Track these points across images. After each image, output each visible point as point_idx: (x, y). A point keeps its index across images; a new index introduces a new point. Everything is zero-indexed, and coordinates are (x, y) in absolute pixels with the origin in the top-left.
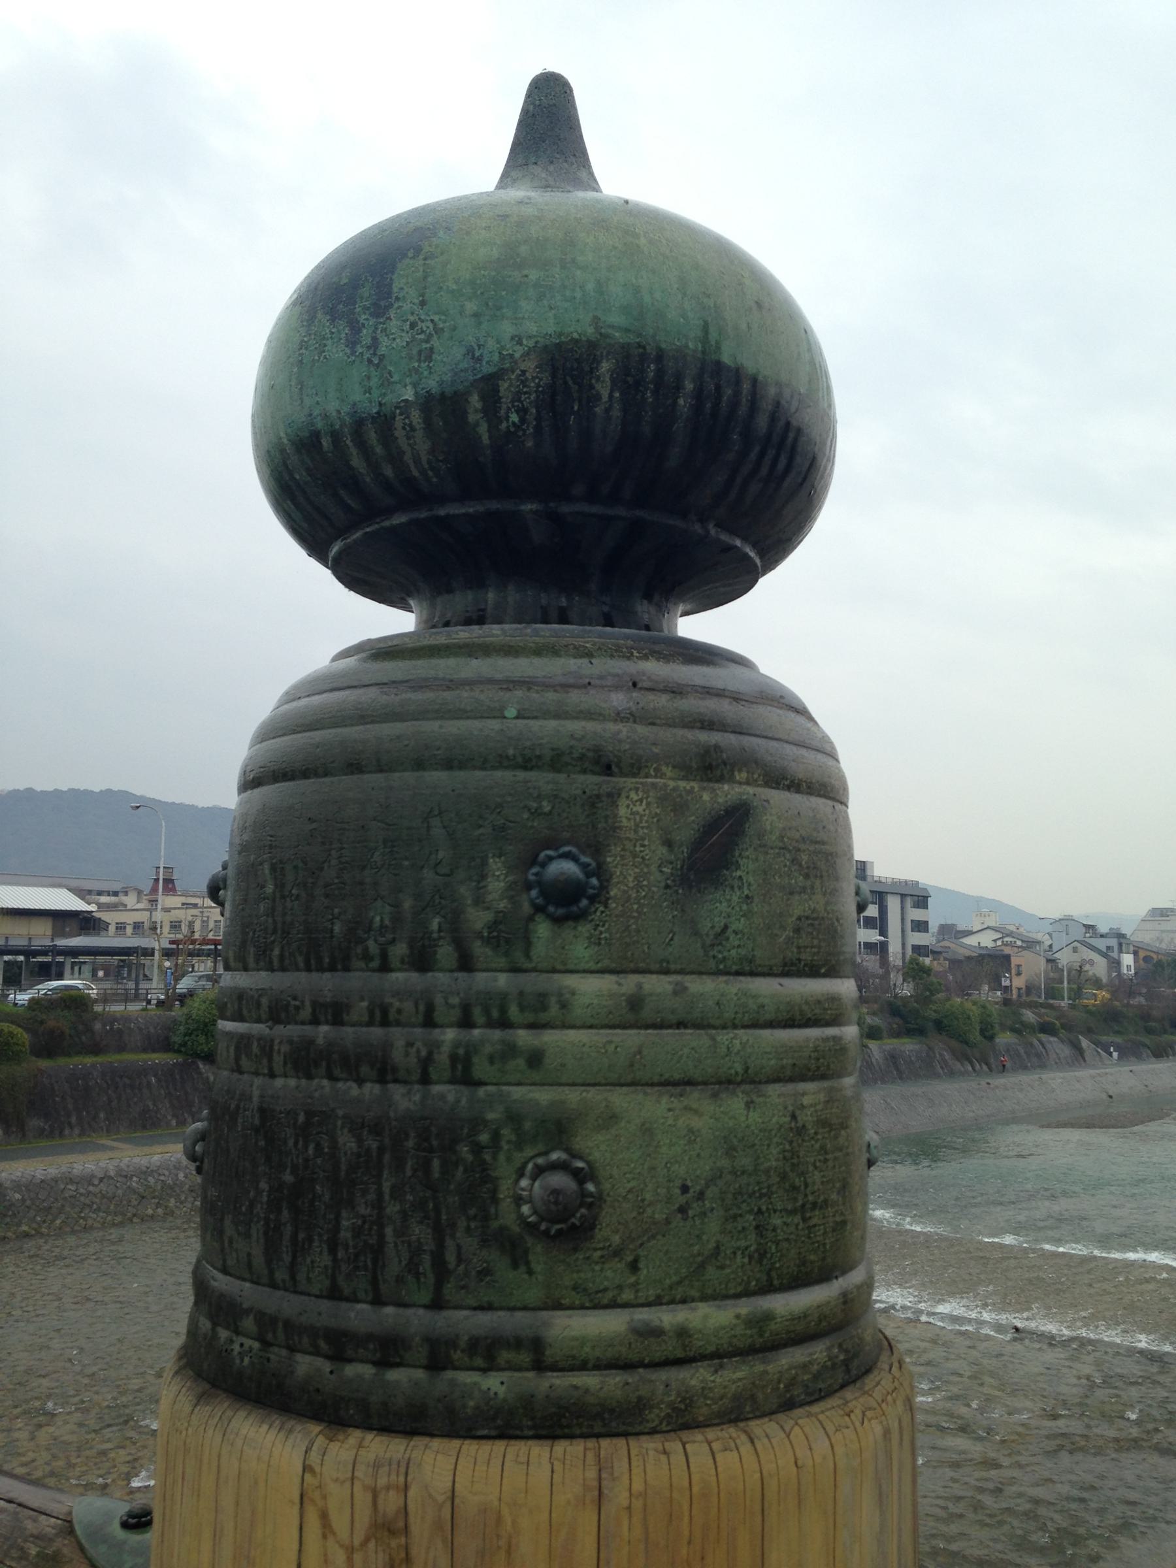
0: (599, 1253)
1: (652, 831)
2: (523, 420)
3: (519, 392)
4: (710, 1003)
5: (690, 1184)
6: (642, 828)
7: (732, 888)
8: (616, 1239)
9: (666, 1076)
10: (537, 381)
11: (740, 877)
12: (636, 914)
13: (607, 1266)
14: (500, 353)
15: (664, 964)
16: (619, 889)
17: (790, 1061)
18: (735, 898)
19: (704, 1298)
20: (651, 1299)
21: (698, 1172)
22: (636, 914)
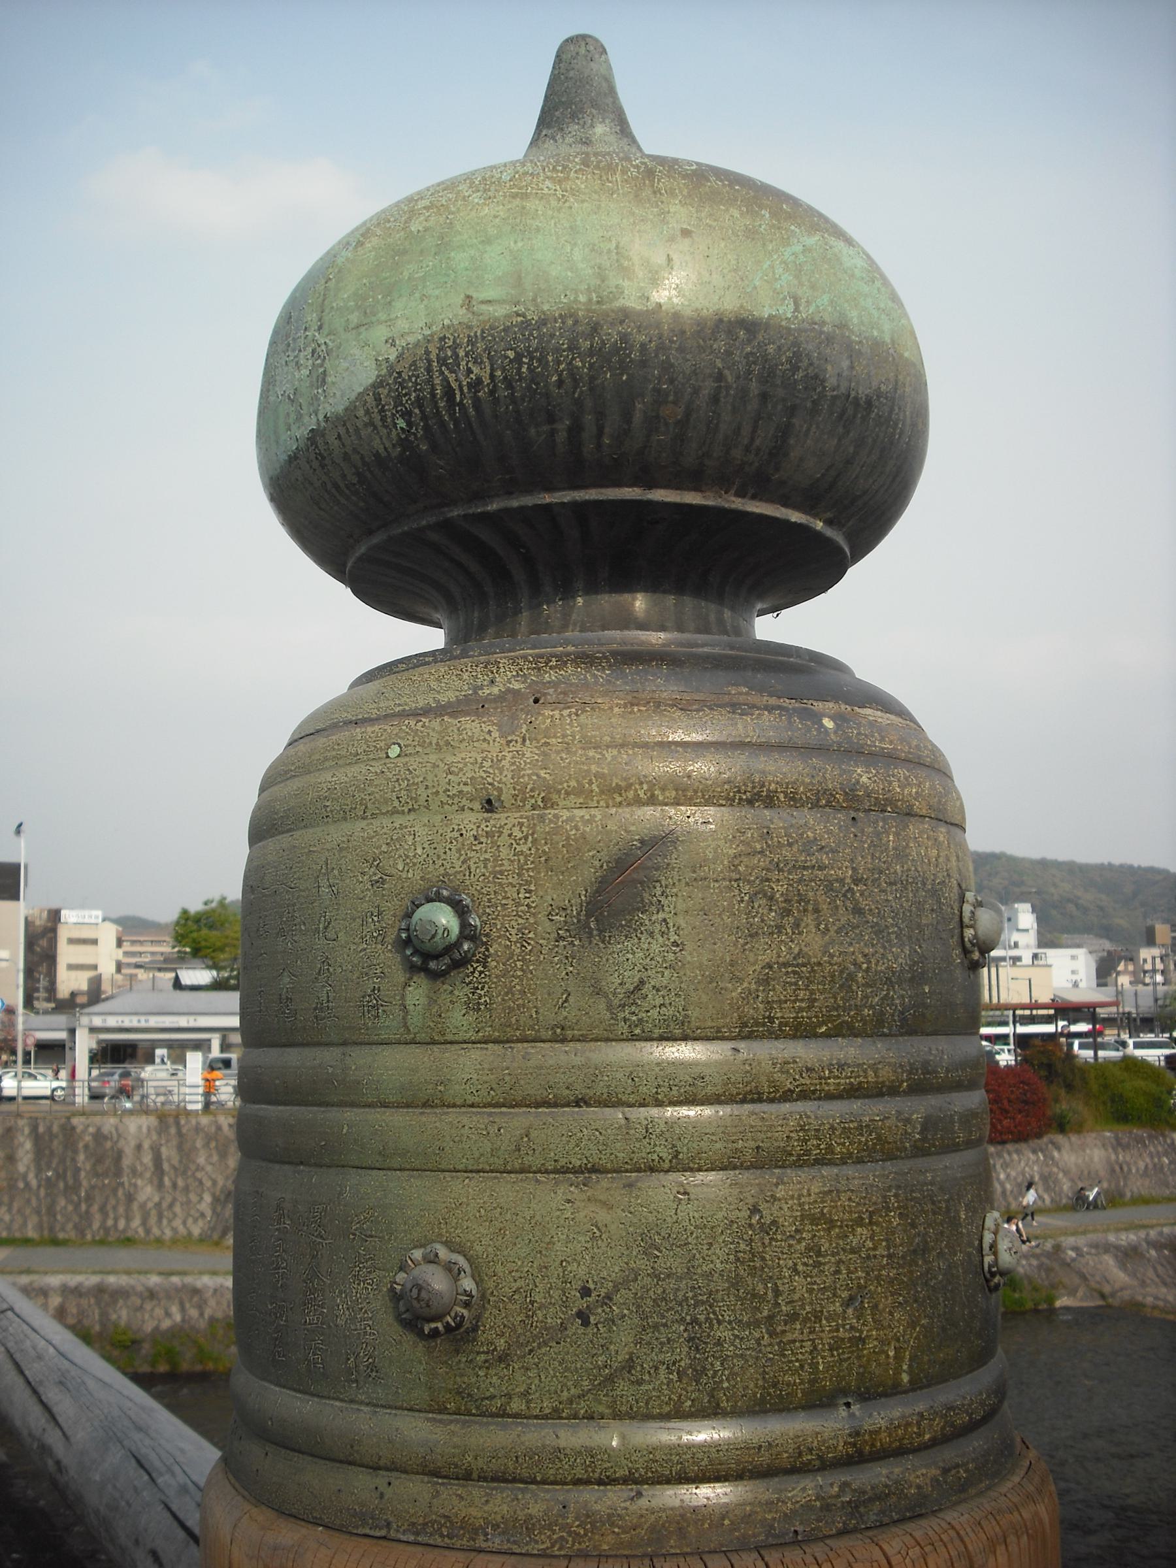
0: (483, 1357)
1: (539, 873)
2: (409, 424)
3: (399, 395)
4: (619, 1075)
5: (592, 1286)
6: (528, 870)
7: (651, 934)
8: (501, 1343)
9: (563, 1162)
10: (413, 379)
11: (665, 920)
12: (519, 973)
13: (492, 1372)
14: (376, 360)
15: (559, 1031)
16: (500, 944)
17: (752, 1144)
18: (655, 948)
19: (617, 1416)
20: (547, 1411)
21: (604, 1274)
22: (519, 973)
